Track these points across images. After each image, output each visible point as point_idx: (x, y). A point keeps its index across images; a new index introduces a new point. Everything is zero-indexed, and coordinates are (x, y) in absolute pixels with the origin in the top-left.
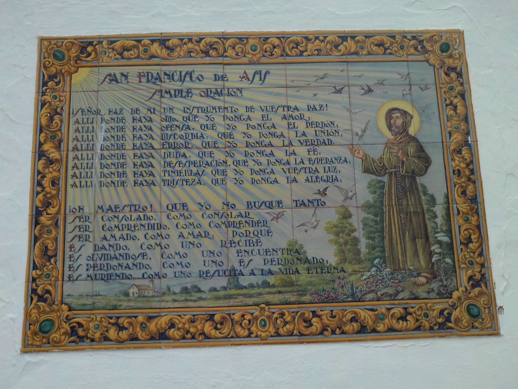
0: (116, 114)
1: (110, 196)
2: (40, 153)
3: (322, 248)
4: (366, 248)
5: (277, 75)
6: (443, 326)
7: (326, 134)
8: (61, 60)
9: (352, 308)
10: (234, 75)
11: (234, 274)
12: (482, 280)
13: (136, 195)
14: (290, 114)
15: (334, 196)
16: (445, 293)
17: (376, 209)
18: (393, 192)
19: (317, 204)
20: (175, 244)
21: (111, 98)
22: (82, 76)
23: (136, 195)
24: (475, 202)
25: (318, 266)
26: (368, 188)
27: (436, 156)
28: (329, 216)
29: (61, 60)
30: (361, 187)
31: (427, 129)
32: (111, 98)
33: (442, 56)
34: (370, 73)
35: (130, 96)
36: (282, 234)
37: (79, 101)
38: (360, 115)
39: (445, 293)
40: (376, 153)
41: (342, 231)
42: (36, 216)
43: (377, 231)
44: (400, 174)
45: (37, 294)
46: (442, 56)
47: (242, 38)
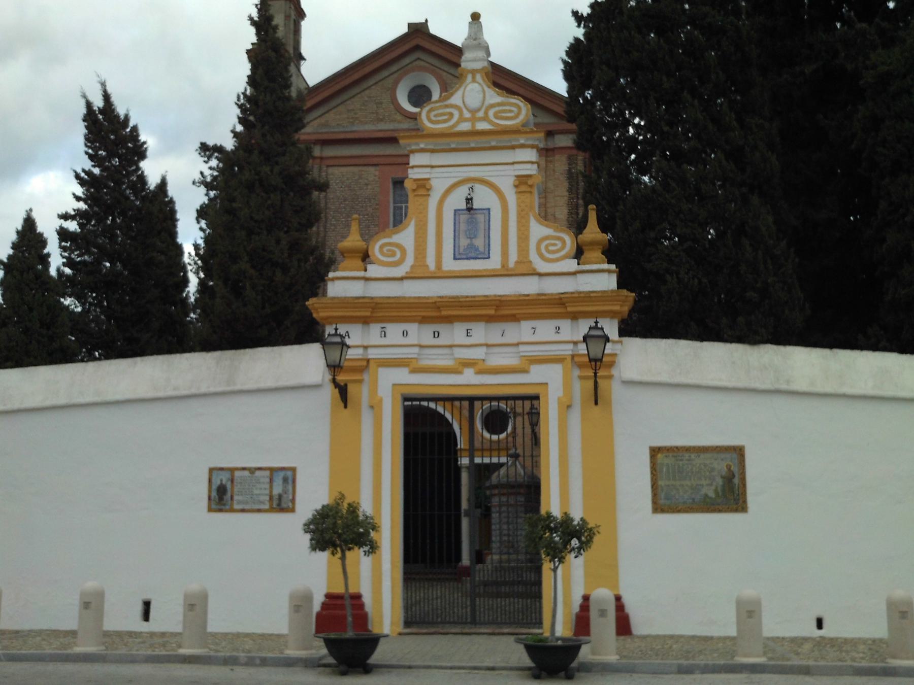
0: (668, 465)
1: (668, 483)
2: (652, 473)
3: (712, 494)
4: (423, 186)
5: (702, 456)
6: (736, 511)
7: (713, 470)
8: (655, 452)
9: (717, 507)
10: (693, 456)
11: (693, 499)
12: (745, 502)
13: (673, 482)
14: (705, 465)
15: (714, 484)
16: (737, 504)
17: (723, 486)
18: (414, 314)
19: (711, 485)
20: (681, 493)
21: (666, 461)
22: (659, 455)
23: (673, 482)
24: (744, 485)
25: (711, 498)
26: (135, 129)
27: (737, 476)
28: (713, 488)
29: (655, 452)
30: (719, 481)
31: (735, 469)
32: (666, 461)
33: (739, 451)
34: (723, 456)
35: (670, 461)
36: (704, 491)
37: (659, 461)
38: (720, 466)
39: (737, 504)
40: (724, 474)
41: (716, 491)
42: (652, 487)
43: (723, 490)
44: (729, 479)
45: (654, 502)
46: (739, 451)
47: (694, 447)
